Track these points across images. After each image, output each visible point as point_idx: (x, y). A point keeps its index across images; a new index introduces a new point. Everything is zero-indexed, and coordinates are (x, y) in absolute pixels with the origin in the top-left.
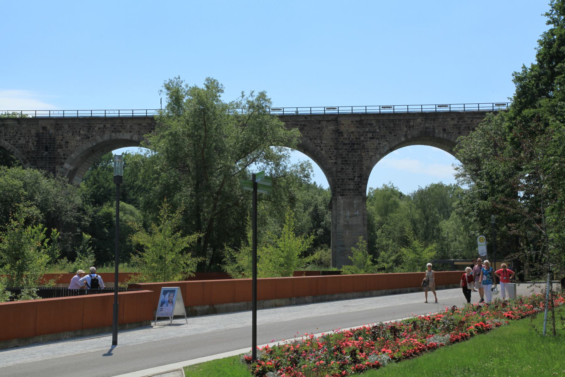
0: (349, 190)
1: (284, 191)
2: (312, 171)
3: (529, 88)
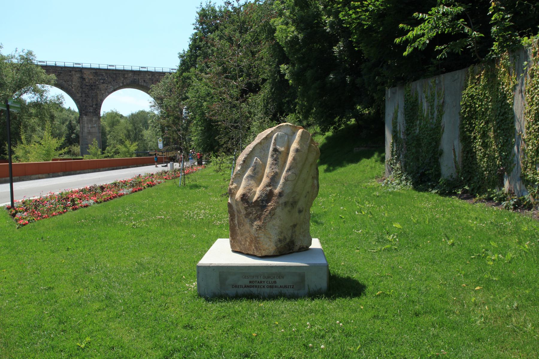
0: (90, 112)
1: (47, 111)
2: (64, 100)
3: (186, 62)
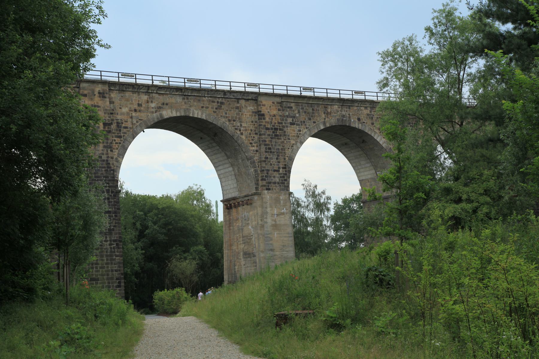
0: (275, 183)
